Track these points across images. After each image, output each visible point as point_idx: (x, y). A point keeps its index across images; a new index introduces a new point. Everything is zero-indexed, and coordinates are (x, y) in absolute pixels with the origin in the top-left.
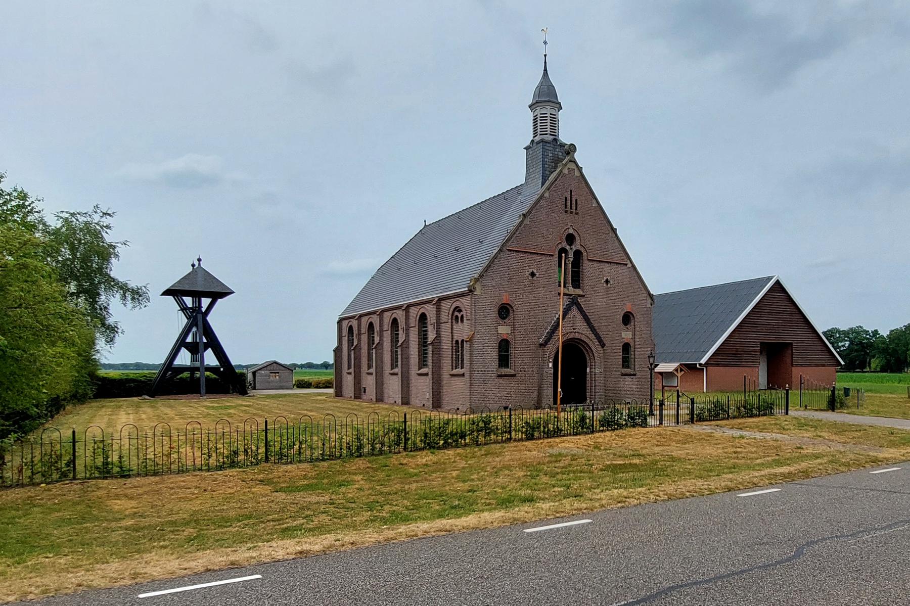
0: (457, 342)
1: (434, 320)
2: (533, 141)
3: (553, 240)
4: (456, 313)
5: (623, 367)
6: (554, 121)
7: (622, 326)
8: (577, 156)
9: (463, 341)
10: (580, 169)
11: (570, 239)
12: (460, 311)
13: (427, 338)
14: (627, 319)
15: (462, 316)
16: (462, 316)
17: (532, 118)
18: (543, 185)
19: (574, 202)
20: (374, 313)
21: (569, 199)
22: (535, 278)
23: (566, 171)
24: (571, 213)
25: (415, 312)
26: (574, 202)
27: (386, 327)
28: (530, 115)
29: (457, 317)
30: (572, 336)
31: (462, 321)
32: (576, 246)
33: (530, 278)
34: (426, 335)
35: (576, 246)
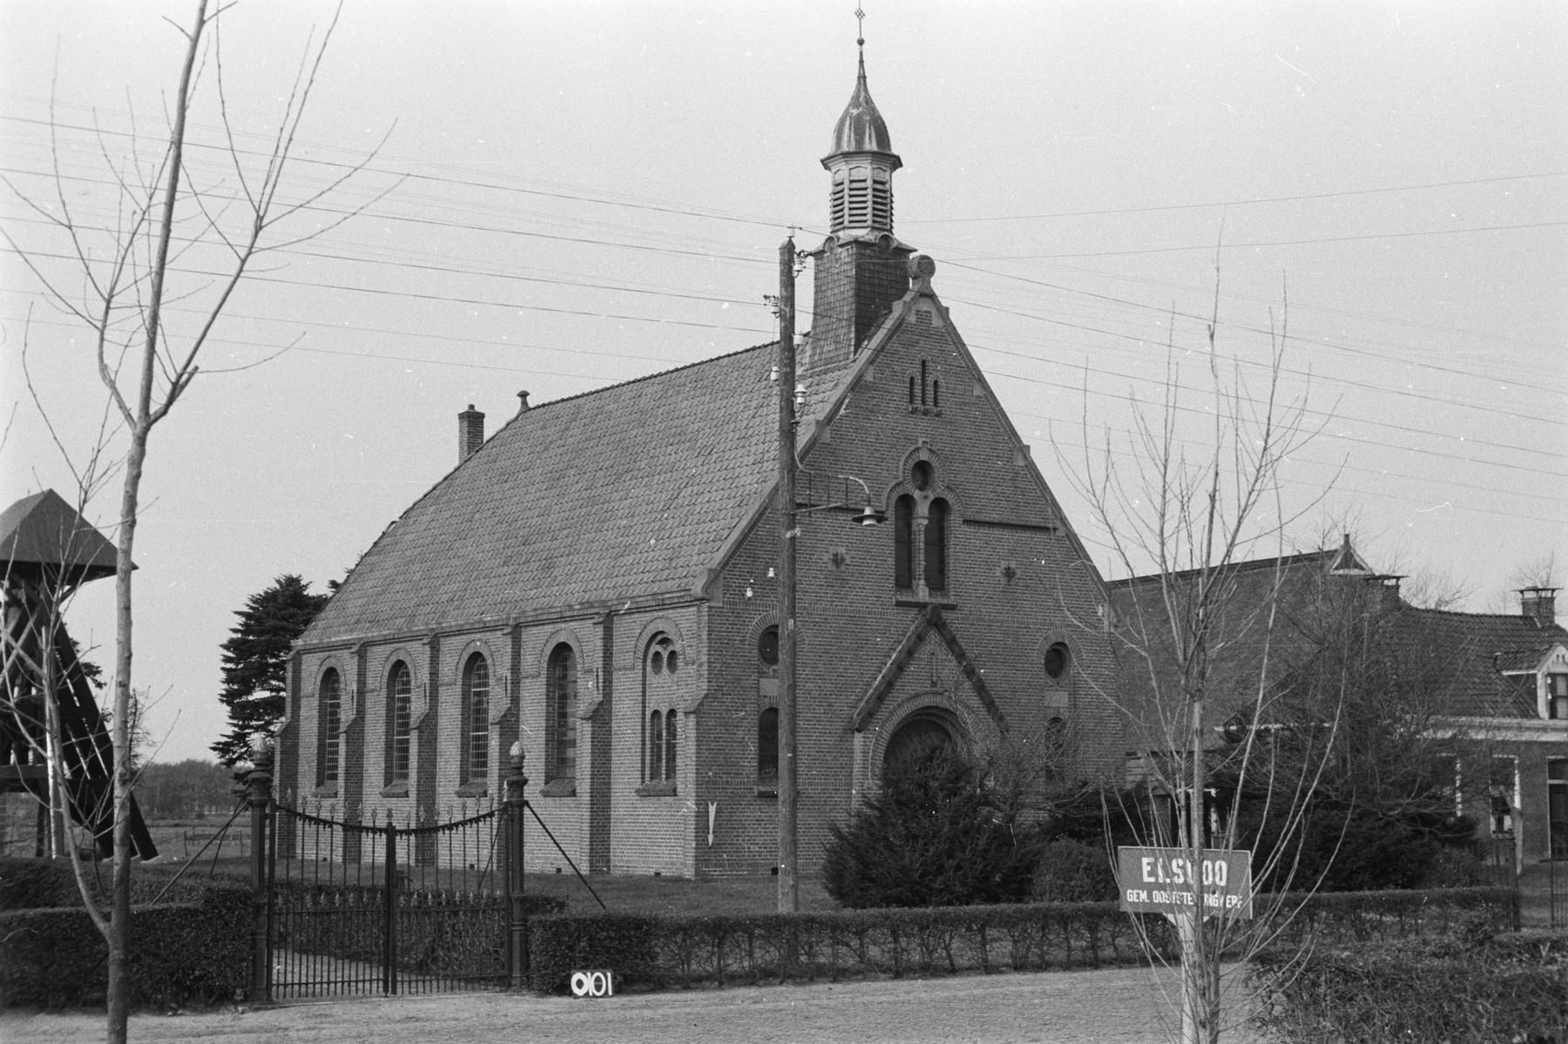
0: (656, 713)
1: (505, 672)
2: (830, 239)
3: (871, 481)
4: (655, 648)
5: (1206, 752)
6: (883, 198)
7: (1050, 681)
8: (937, 284)
9: (672, 713)
10: (944, 312)
11: (923, 471)
12: (665, 641)
13: (408, 716)
14: (1057, 658)
15: (673, 654)
16: (673, 654)
17: (830, 189)
18: (858, 346)
19: (930, 389)
20: (346, 646)
21: (918, 381)
22: (843, 568)
23: (912, 319)
24: (925, 413)
25: (538, 644)
26: (930, 389)
27: (371, 682)
28: (826, 180)
29: (657, 654)
30: (927, 701)
31: (672, 664)
32: (938, 490)
33: (831, 566)
34: (336, 713)
35: (938, 490)
